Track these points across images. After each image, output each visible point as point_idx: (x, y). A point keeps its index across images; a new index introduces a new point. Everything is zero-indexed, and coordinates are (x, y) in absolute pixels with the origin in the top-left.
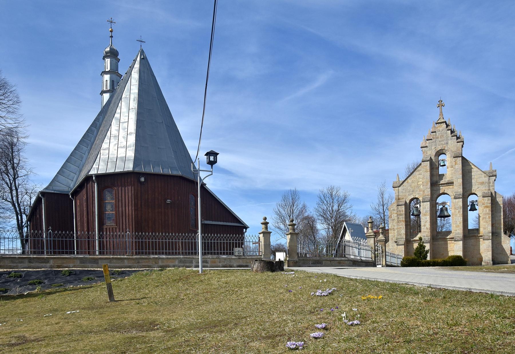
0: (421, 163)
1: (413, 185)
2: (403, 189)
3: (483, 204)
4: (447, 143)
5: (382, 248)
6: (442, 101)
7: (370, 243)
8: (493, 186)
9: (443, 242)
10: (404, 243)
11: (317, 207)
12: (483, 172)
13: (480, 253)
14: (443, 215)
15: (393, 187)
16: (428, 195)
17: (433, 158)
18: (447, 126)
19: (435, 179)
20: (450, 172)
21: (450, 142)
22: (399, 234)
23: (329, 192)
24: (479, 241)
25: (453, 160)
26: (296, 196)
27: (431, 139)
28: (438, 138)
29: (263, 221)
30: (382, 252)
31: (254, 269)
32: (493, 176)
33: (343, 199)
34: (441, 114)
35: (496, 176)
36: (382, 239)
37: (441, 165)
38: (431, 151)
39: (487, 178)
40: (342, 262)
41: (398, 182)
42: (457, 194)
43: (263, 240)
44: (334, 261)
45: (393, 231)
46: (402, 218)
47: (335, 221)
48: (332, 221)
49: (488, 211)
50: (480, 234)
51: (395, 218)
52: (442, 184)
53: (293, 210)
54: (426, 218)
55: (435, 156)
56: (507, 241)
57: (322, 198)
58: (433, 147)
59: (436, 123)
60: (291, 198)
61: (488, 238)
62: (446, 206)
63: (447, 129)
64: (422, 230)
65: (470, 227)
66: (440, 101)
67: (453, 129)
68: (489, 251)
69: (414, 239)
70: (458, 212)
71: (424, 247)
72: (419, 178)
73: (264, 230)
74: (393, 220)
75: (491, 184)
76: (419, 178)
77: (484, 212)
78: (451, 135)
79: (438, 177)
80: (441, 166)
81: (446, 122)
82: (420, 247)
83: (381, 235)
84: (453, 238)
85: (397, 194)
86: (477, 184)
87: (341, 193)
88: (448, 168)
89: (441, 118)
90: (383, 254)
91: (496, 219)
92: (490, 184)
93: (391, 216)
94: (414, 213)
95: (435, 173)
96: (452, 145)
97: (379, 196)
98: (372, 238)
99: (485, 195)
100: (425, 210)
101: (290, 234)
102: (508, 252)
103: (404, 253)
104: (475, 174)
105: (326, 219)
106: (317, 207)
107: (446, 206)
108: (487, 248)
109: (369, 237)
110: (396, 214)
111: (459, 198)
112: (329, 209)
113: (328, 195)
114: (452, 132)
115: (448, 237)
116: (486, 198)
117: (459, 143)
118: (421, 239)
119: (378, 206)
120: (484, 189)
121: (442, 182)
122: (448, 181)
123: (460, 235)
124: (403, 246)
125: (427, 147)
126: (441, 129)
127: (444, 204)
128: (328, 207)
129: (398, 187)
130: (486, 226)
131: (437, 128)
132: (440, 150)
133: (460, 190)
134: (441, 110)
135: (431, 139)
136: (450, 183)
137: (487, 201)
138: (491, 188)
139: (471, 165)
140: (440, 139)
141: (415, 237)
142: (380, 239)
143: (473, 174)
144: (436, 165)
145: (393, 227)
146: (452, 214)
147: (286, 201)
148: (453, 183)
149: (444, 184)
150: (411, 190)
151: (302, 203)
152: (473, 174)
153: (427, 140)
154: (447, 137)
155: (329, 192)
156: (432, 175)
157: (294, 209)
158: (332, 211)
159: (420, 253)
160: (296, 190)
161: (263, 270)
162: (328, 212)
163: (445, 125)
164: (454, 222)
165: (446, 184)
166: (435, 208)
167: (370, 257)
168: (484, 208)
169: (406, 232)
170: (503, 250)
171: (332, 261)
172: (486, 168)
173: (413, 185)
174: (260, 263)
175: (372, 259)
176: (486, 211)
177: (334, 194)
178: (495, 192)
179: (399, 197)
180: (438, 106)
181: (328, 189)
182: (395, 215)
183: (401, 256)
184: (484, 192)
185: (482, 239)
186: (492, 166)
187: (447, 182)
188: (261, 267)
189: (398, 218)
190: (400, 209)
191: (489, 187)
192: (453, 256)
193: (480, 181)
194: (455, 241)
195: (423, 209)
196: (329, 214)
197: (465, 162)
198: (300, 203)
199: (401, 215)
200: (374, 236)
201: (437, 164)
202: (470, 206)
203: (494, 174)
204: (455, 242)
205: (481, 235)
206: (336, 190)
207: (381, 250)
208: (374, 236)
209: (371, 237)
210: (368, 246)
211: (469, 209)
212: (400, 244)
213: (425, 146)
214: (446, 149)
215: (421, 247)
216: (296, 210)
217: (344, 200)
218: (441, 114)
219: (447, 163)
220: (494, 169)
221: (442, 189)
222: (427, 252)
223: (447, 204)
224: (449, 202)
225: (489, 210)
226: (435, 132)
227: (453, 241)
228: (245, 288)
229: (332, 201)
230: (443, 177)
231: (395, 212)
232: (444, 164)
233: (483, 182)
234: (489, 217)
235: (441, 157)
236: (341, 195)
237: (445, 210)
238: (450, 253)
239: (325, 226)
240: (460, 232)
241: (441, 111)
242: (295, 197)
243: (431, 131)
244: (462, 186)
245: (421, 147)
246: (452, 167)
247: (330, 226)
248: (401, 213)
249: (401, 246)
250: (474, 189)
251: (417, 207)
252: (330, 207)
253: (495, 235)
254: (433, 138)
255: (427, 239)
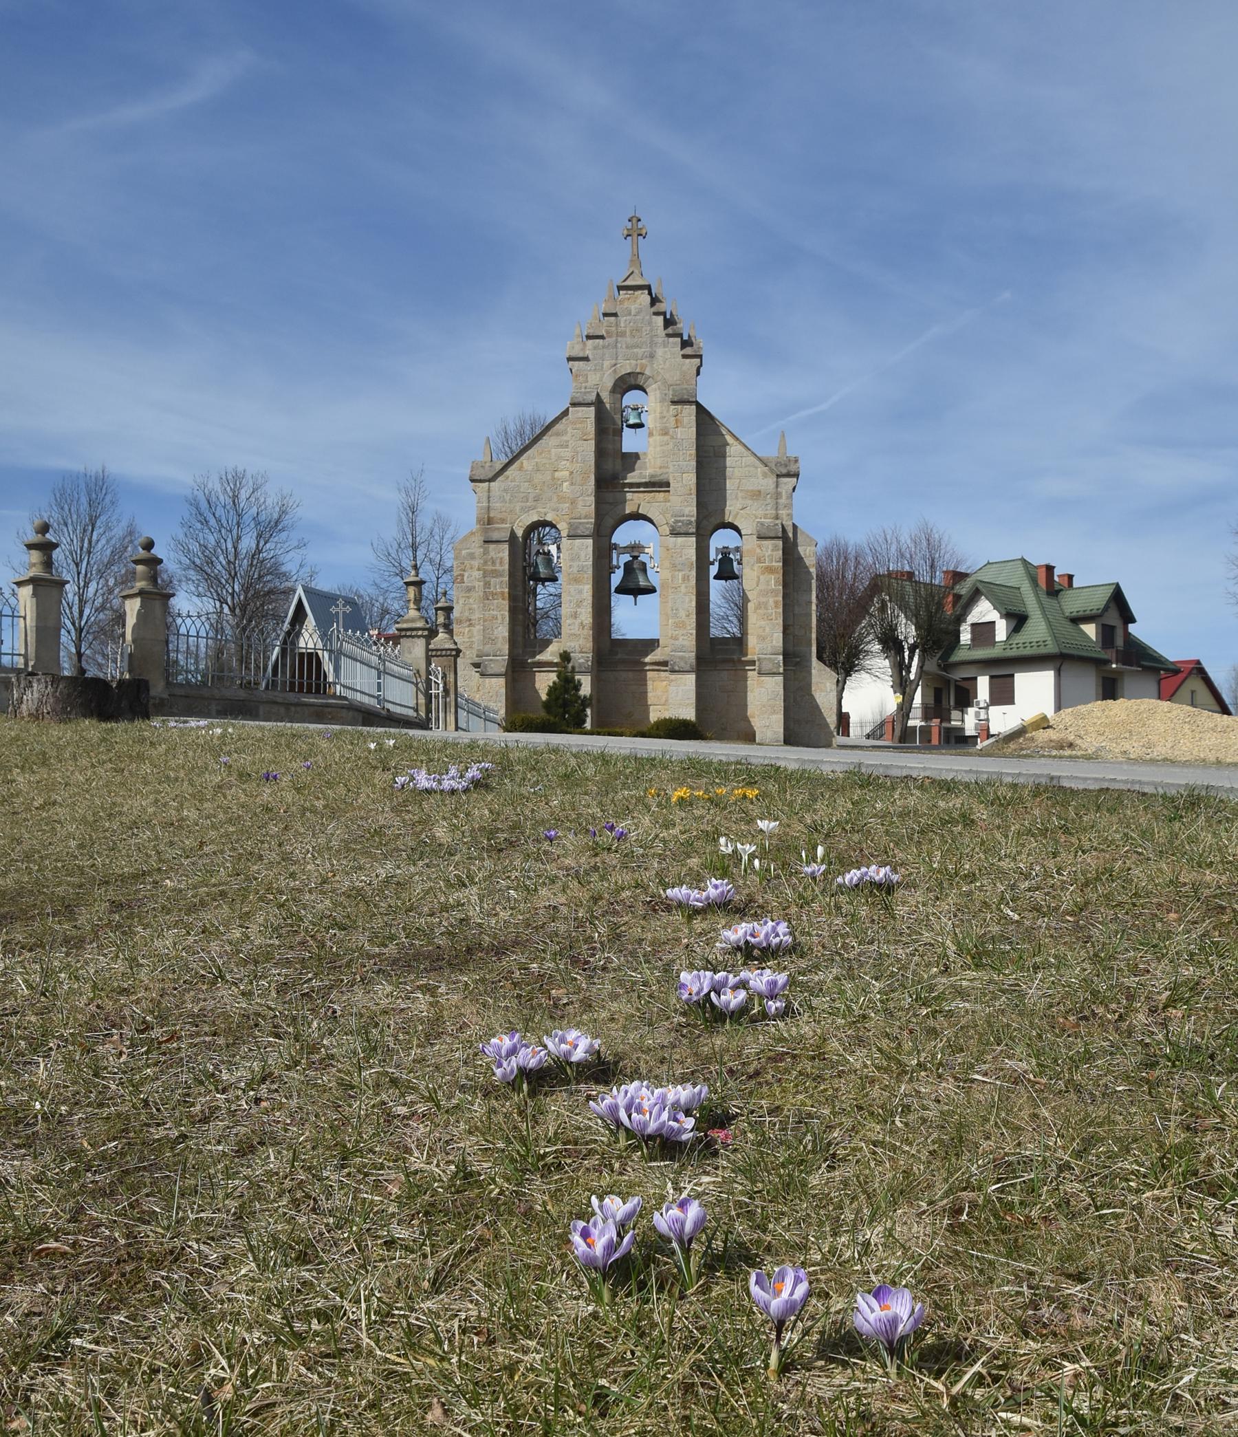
0: (568, 409)
1: (538, 478)
2: (505, 490)
3: (759, 560)
4: (652, 356)
5: (445, 676)
6: (639, 220)
7: (413, 655)
8: (789, 506)
9: (631, 675)
10: (503, 670)
11: (181, 537)
12: (760, 459)
13: (747, 717)
14: (631, 585)
15: (473, 481)
16: (586, 517)
17: (606, 397)
18: (654, 301)
19: (611, 465)
20: (658, 449)
21: (660, 352)
22: (488, 639)
23: (228, 489)
24: (745, 679)
25: (668, 411)
26: (104, 492)
27: (602, 337)
28: (623, 334)
29: (33, 538)
30: (446, 691)
31: (24, 707)
32: (788, 475)
33: (276, 516)
34: (636, 259)
35: (796, 475)
36: (447, 646)
37: (632, 421)
38: (598, 375)
39: (770, 482)
40: (330, 713)
41: (488, 464)
42: (680, 521)
43: (31, 611)
44: (299, 709)
45: (467, 629)
46: (501, 585)
47: (246, 589)
48: (233, 588)
49: (774, 582)
50: (747, 655)
51: (477, 584)
52: (631, 485)
53: (90, 542)
54: (580, 592)
55: (614, 390)
56: (828, 684)
57: (204, 505)
58: (607, 364)
59: (620, 288)
60: (84, 500)
61: (775, 670)
62: (642, 558)
63: (654, 309)
64: (565, 630)
65: (715, 632)
66: (634, 220)
67: (671, 314)
68: (774, 712)
69: (538, 657)
70: (684, 579)
71: (577, 686)
72: (560, 458)
73: (35, 572)
74: (469, 589)
75: (783, 501)
76: (560, 458)
77: (762, 587)
78: (666, 332)
79: (619, 461)
80: (630, 426)
81: (648, 288)
82: (562, 683)
83: (440, 635)
84: (665, 663)
85: (485, 504)
86: (740, 494)
87: (271, 499)
88: (651, 434)
89: (636, 271)
90: (448, 700)
91: (796, 612)
92: (779, 501)
93: (460, 575)
94: (539, 572)
95: (610, 446)
96: (668, 357)
97: (402, 516)
98: (419, 637)
99: (764, 532)
100: (575, 564)
101: (141, 593)
102: (832, 720)
103: (504, 705)
104: (735, 458)
105: (212, 581)
106: (181, 537)
107: (642, 558)
108: (769, 700)
109: (408, 633)
110: (479, 569)
111: (687, 534)
112: (224, 548)
113: (222, 498)
114: (669, 322)
115: (647, 660)
116: (768, 544)
117: (688, 361)
118: (565, 657)
119: (395, 546)
120: (760, 512)
121: (632, 478)
122: (652, 476)
123: (686, 655)
124: (502, 681)
125: (586, 359)
126: (633, 308)
127: (635, 549)
128: (222, 541)
129: (490, 480)
130: (767, 629)
131: (621, 302)
132: (629, 374)
133: (690, 510)
134: (635, 247)
135: (602, 337)
136: (659, 485)
137: (770, 553)
138: (783, 512)
139: (724, 433)
140: (628, 340)
141: (540, 652)
142: (439, 647)
143: (729, 461)
144: (614, 423)
145: (467, 614)
146: (662, 586)
147: (66, 507)
148: (668, 484)
149: (638, 485)
150: (531, 497)
151: (124, 523)
152: (728, 464)
153: (589, 337)
154: (652, 337)
155: (228, 489)
156: (600, 453)
157: (95, 537)
158: (236, 555)
159: (566, 705)
160: (106, 474)
161: (64, 710)
162: (221, 558)
163: (648, 298)
164: (670, 612)
165: (646, 485)
166: (607, 561)
167: (412, 703)
168: (763, 573)
169: (512, 632)
170: (816, 708)
171: (293, 709)
172: (770, 452)
173: (538, 478)
174: (52, 682)
175: (416, 710)
176: (768, 582)
177: (243, 495)
178: (795, 527)
179: (491, 515)
180: (626, 232)
181: (224, 478)
182: (477, 574)
183: (496, 713)
184: (762, 524)
185: (756, 673)
186: (785, 445)
187: (647, 480)
188: (57, 700)
189: (487, 585)
190: (492, 554)
191: (777, 509)
192: (670, 720)
193: (751, 488)
194: (673, 671)
195: (572, 560)
196: (224, 562)
197: (705, 419)
198: (119, 521)
199: (496, 574)
200: (426, 633)
201: (617, 417)
202: (717, 564)
203: (793, 468)
204: (673, 677)
205: (749, 657)
206: (251, 483)
207: (441, 686)
208: (426, 633)
209: (414, 633)
210: (406, 666)
211: (712, 576)
212: (490, 671)
213: (581, 355)
214: (647, 372)
215: (567, 684)
216: (103, 541)
217: (270, 528)
218: (636, 259)
219: (648, 419)
220: (791, 453)
221: (634, 501)
222: (585, 702)
223: (646, 550)
224: (651, 545)
225: (776, 582)
226: (615, 315)
227: (667, 674)
228: (23, 768)
229: (235, 521)
230: (635, 462)
231: (476, 563)
232: (637, 421)
233: (760, 491)
234: (776, 603)
235: (631, 398)
236: (269, 502)
237: (640, 569)
238: (654, 711)
239: (209, 605)
240: (685, 643)
241: (635, 250)
242: (101, 496)
243: (602, 311)
244: (694, 497)
245: (570, 359)
246: (666, 434)
247: (224, 605)
248: (498, 567)
249: (494, 680)
250: (733, 510)
251: (549, 551)
252: (229, 540)
253: (793, 662)
254: (608, 332)
255: (582, 661)
